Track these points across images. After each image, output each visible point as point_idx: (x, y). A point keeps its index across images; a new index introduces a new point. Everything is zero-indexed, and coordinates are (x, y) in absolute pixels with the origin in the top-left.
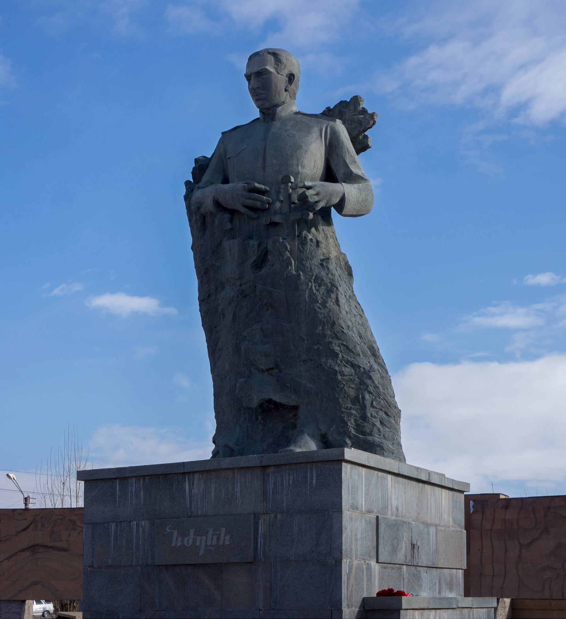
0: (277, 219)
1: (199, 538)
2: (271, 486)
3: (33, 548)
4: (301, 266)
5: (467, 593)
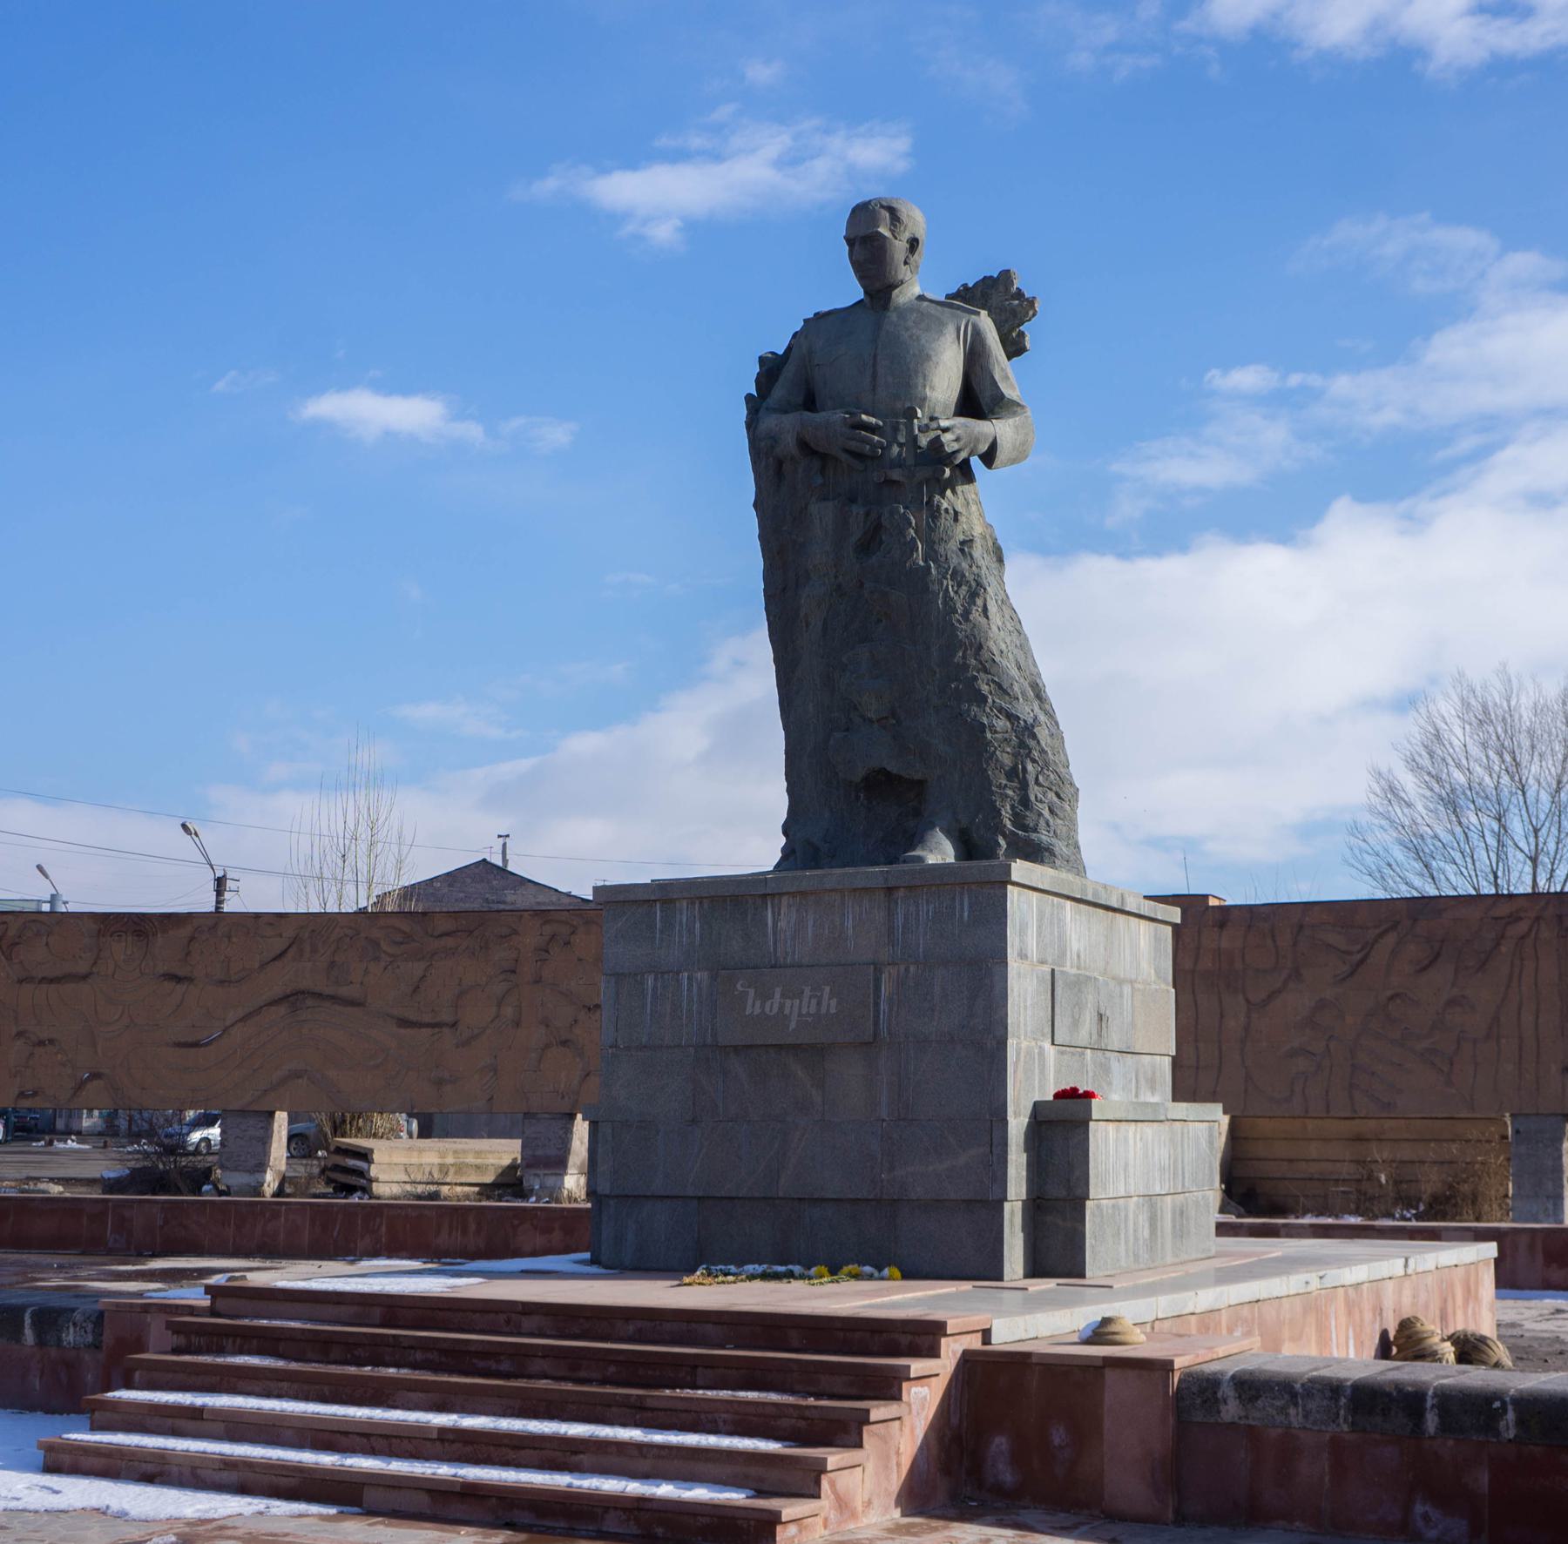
0: (896, 475)
1: (788, 1003)
2: (900, 920)
3: (293, 998)
4: (931, 554)
5: (1177, 1097)
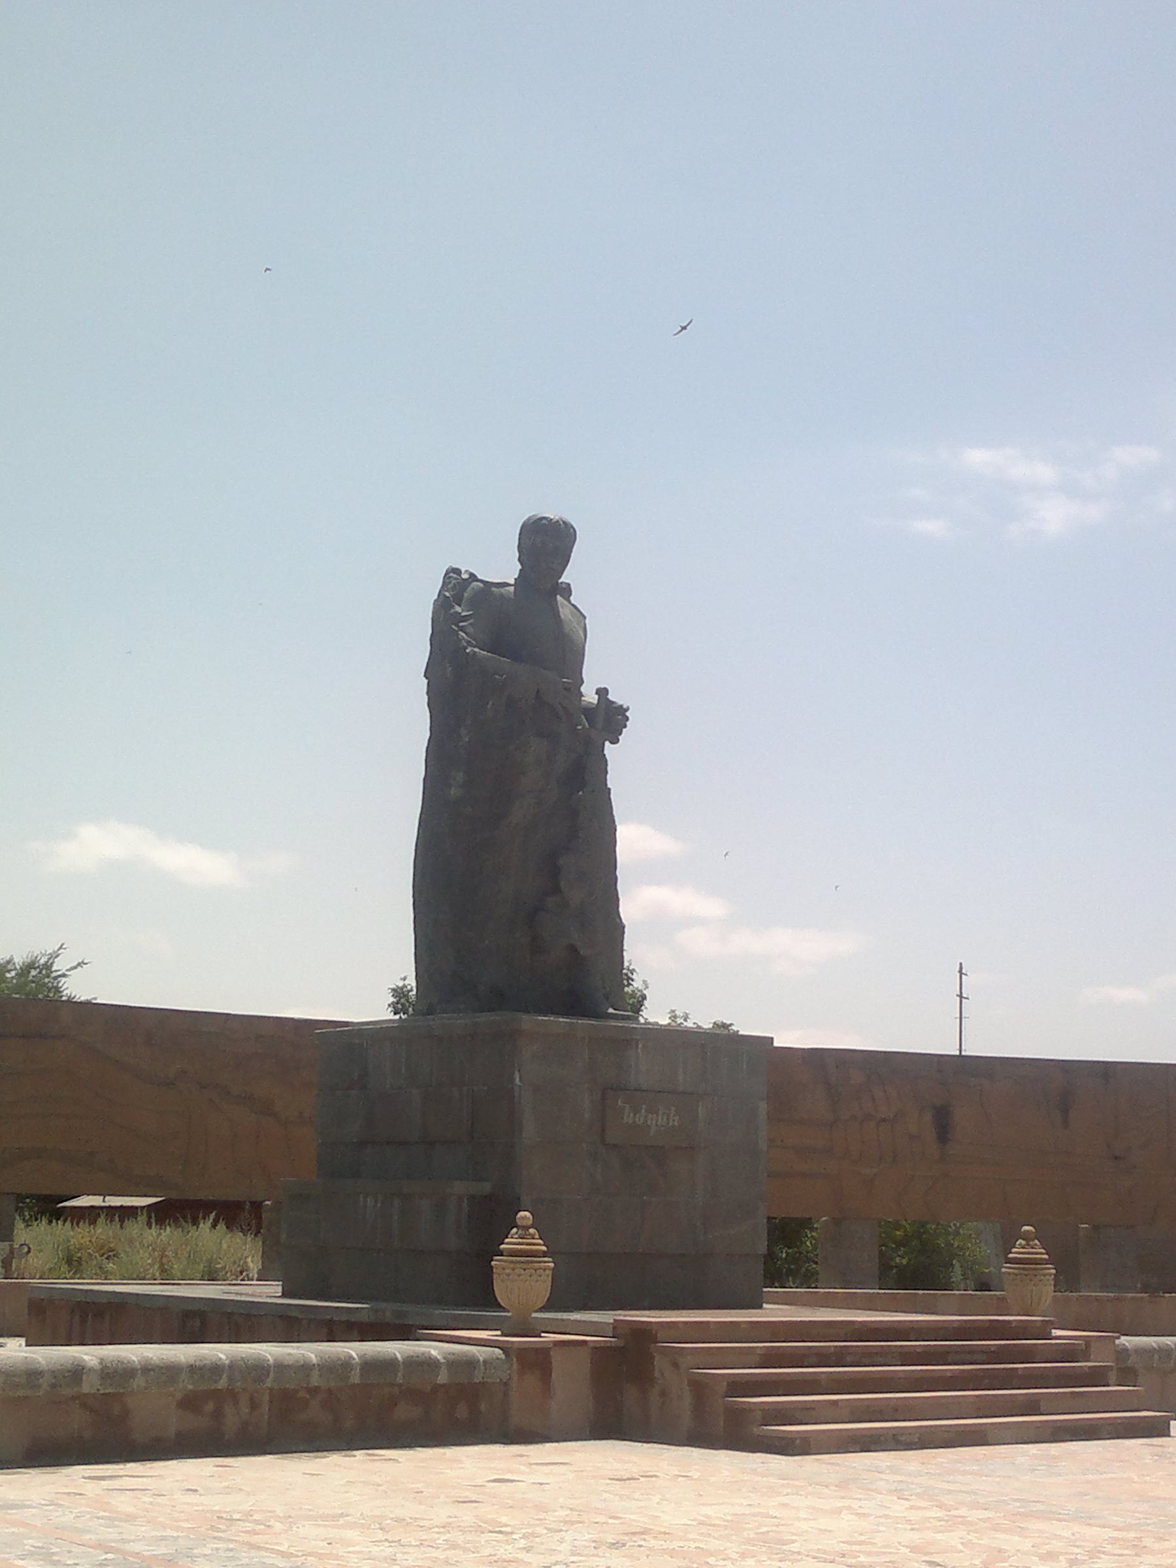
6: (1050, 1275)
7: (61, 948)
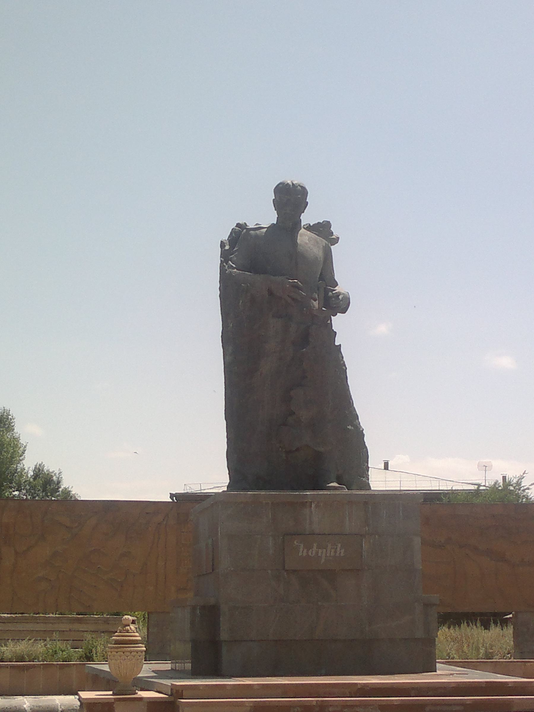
1: (320, 551)
6: (142, 651)
7: (524, 474)
